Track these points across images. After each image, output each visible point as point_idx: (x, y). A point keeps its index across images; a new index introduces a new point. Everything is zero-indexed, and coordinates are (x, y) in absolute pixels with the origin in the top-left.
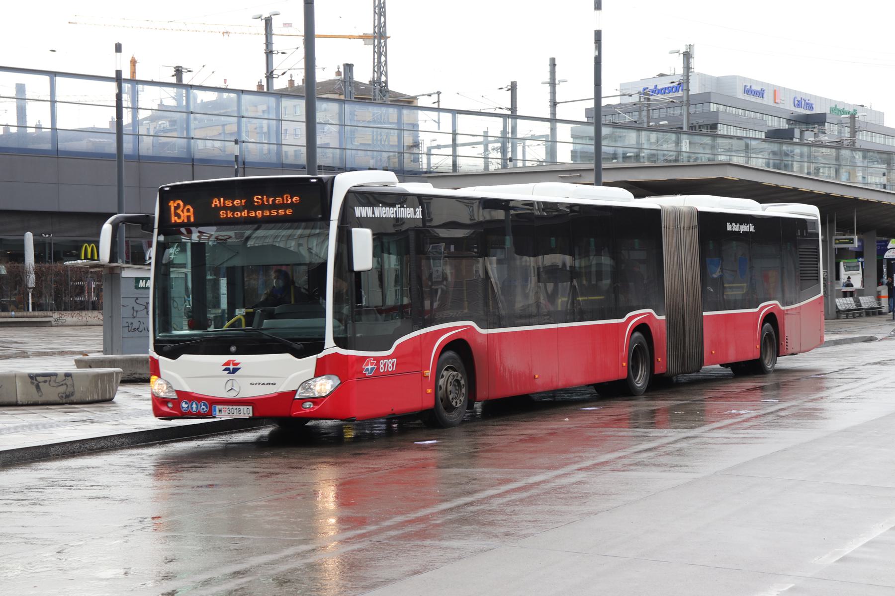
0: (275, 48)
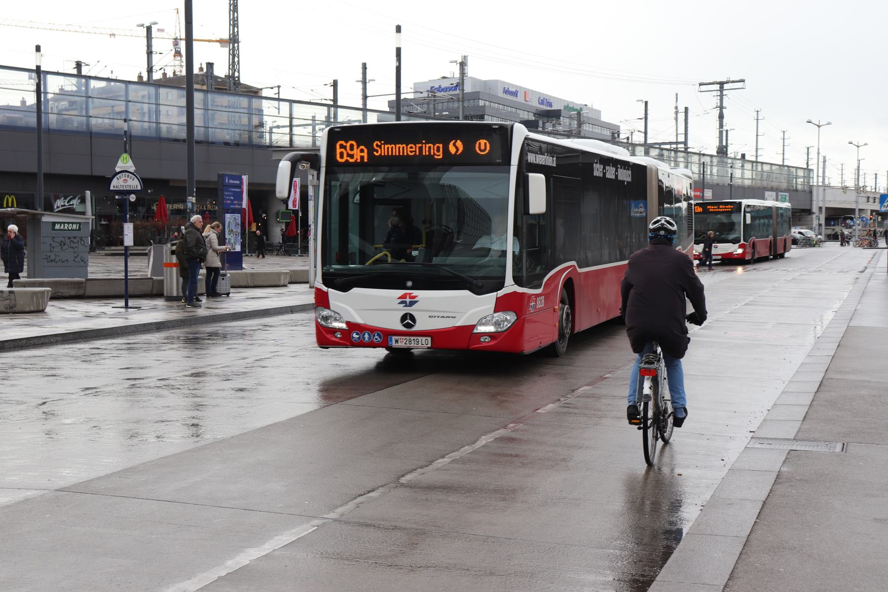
0: (154, 49)
